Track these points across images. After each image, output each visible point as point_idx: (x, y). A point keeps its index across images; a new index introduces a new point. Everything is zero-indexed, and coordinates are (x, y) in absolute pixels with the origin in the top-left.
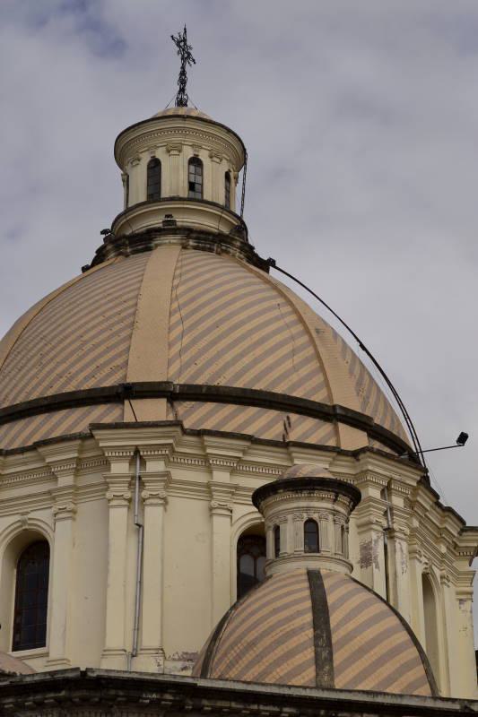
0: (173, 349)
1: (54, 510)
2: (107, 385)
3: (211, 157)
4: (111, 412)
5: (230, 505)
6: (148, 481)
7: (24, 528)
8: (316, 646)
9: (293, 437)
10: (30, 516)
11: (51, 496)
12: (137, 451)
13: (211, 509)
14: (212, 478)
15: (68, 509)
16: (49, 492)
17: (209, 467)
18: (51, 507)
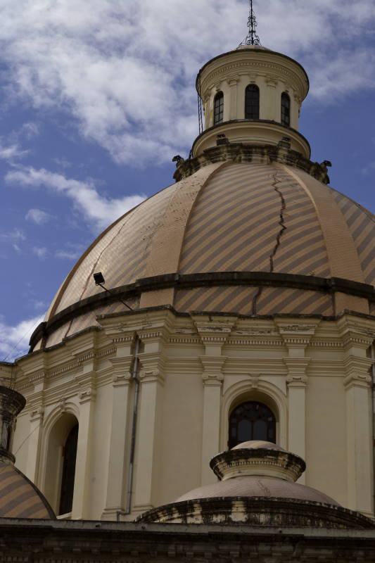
2: (190, 273)
3: (267, 82)
4: (201, 295)
7: (253, 387)
9: (249, 291)
12: (137, 337)
13: (287, 383)
15: (154, 374)
17: (285, 345)
18: (286, 375)
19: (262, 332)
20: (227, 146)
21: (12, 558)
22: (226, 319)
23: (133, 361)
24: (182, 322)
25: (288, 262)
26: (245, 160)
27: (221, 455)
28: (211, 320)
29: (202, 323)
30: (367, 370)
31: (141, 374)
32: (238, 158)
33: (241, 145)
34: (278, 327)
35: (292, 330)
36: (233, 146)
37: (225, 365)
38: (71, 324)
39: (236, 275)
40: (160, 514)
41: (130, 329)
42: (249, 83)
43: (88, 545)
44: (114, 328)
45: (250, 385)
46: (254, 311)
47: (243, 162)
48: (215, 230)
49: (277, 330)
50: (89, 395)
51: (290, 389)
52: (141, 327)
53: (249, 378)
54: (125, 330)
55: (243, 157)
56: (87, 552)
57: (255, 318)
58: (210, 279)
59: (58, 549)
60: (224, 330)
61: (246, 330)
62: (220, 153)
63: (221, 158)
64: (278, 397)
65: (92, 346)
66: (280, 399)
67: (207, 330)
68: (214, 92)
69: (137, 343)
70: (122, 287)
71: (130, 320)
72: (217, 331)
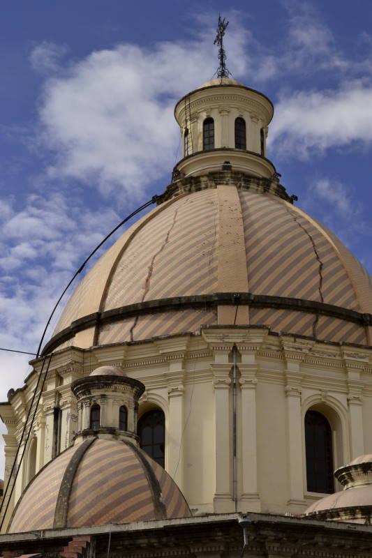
0: (251, 266)
5: (300, 389)
6: (244, 371)
8: (55, 515)
9: (309, 317)
10: (329, 394)
11: (167, 378)
12: (235, 348)
13: (348, 400)
14: (286, 368)
15: (253, 382)
16: (165, 375)
19: (330, 356)
20: (232, 173)
21: (203, 549)
22: (307, 341)
23: (233, 368)
24: (272, 339)
26: (244, 187)
28: (295, 341)
29: (288, 343)
31: (241, 381)
32: (239, 185)
33: (243, 174)
35: (353, 357)
36: (237, 173)
37: (304, 380)
38: (137, 320)
39: (299, 302)
40: (342, 513)
41: (230, 341)
42: (238, 116)
43: (343, 542)
44: (216, 338)
45: (321, 399)
46: (314, 334)
47: (242, 188)
49: (341, 355)
50: (180, 391)
51: (351, 406)
52: (241, 340)
53: (320, 393)
54: (226, 340)
55: (243, 185)
56: (341, 547)
57: (326, 344)
60: (304, 351)
62: (225, 177)
63: (225, 182)
64: (341, 410)
65: (184, 348)
67: (291, 349)
68: (204, 116)
69: (235, 352)
70: (192, 297)
72: (299, 351)
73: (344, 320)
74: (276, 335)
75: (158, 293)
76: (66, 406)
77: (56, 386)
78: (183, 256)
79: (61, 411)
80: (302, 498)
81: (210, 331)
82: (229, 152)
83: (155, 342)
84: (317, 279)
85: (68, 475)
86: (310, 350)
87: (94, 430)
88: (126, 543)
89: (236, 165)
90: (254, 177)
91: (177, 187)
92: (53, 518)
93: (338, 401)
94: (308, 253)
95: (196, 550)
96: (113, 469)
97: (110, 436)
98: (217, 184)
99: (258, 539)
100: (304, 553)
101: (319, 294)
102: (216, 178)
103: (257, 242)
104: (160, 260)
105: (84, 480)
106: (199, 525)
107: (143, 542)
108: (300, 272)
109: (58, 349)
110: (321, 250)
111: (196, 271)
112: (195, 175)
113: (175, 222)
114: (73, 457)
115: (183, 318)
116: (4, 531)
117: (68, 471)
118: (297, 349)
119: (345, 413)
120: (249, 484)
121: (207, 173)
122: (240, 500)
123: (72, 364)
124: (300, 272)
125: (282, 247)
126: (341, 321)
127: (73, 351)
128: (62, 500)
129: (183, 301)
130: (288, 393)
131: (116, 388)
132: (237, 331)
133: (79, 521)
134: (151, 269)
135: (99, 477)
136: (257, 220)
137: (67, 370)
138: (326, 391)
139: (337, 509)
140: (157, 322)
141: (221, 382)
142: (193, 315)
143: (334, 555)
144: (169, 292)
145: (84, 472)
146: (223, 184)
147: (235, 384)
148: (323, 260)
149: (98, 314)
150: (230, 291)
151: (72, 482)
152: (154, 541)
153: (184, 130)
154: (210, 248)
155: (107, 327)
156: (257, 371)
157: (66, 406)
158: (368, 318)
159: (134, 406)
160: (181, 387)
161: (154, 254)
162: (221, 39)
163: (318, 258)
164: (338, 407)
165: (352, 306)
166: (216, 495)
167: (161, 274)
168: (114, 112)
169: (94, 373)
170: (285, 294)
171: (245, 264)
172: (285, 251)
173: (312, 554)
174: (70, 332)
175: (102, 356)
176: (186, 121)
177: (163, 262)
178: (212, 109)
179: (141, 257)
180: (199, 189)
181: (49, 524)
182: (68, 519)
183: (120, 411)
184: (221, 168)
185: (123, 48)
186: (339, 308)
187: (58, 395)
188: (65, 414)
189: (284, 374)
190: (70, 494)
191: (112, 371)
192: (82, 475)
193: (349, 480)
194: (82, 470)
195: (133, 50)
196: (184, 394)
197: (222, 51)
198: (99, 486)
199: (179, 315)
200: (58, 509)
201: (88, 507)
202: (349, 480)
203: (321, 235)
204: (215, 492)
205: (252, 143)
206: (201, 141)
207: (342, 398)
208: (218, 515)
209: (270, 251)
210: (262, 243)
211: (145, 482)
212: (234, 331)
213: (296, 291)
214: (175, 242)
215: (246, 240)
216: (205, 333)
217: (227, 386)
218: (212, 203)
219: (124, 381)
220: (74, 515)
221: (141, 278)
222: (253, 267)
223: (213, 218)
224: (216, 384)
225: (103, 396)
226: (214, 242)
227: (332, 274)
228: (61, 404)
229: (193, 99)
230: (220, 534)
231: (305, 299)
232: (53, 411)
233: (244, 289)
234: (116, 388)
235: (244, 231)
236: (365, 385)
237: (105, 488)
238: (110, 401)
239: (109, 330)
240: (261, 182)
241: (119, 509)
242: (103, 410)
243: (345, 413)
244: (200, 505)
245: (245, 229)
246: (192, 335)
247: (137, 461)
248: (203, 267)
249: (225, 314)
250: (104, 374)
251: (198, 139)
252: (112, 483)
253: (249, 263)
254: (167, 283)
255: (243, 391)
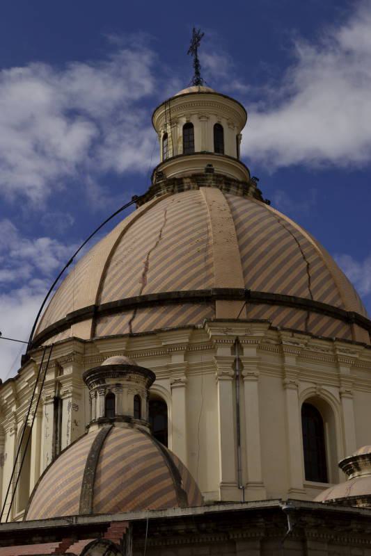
1: (172, 379)
5: (297, 381)
8: (81, 502)
9: (300, 314)
10: (323, 387)
11: (169, 370)
12: (237, 340)
13: (340, 393)
15: (230, 374)
16: (167, 367)
19: (323, 351)
20: (214, 175)
23: (235, 361)
24: (272, 334)
25: (260, 279)
26: (225, 189)
27: (367, 455)
28: (293, 336)
29: (286, 337)
30: (231, 365)
31: (244, 373)
33: (225, 177)
34: (336, 348)
36: (219, 176)
38: (135, 313)
40: (359, 501)
41: (234, 334)
44: (220, 331)
45: (315, 392)
48: (277, 255)
49: (334, 350)
51: (343, 399)
53: (314, 386)
54: (229, 334)
55: (224, 187)
57: (321, 339)
58: (274, 299)
59: (356, 530)
61: (313, 347)
62: (207, 180)
63: (207, 184)
65: (187, 340)
66: (336, 407)
68: (184, 121)
69: (237, 345)
71: (235, 327)
72: (296, 345)
73: (333, 317)
74: (274, 329)
75: (155, 286)
76: (68, 395)
77: (56, 376)
78: (179, 252)
79: (62, 400)
80: (301, 487)
81: (214, 324)
82: (209, 156)
83: (158, 335)
84: (305, 278)
85: (91, 461)
86: (306, 345)
87: (110, 417)
88: (164, 529)
89: (218, 169)
90: (234, 181)
91: (160, 188)
92: (78, 504)
93: (331, 394)
94: (295, 253)
95: (236, 537)
96: (134, 456)
97: (126, 424)
98: (199, 186)
99: (297, 525)
100: (338, 539)
101: (309, 292)
102: (199, 180)
103: (249, 241)
104: (156, 255)
105: (107, 467)
106: (240, 511)
107: (181, 528)
108: (289, 272)
109: (49, 342)
110: (306, 250)
111: (192, 267)
112: (177, 177)
113: (166, 220)
114: (94, 444)
115: (182, 312)
116: (3, 520)
117: (89, 458)
118: (294, 343)
119: (338, 405)
120: (254, 473)
121: (191, 175)
122: (246, 488)
123: (74, 354)
124: (289, 272)
125: (272, 246)
126: (330, 318)
127: (75, 342)
128: (86, 486)
129: (182, 296)
130: (287, 386)
131: (130, 377)
132: (240, 324)
133: (105, 507)
134: (147, 264)
135: (122, 465)
136: (246, 220)
137: (67, 360)
138: (320, 385)
139: (354, 497)
140: (156, 316)
141: (224, 374)
142: (192, 309)
143: (365, 540)
144: (166, 287)
145: (107, 460)
146: (205, 186)
147: (237, 376)
148: (310, 260)
149: (96, 307)
150: (227, 287)
151: (96, 469)
152: (193, 527)
153: (162, 134)
154: (204, 246)
155: (105, 319)
156: (258, 364)
157: (68, 395)
158: (354, 316)
159: (146, 396)
160: (184, 378)
161: (148, 250)
162: (196, 50)
163: (304, 258)
164: (332, 400)
165: (337, 304)
166: (222, 483)
167: (158, 268)
168: (24, 126)
169: (106, 363)
170: (278, 291)
171: (240, 261)
172: (274, 251)
173: (346, 540)
174: (65, 324)
175: (103, 348)
176: (166, 125)
177: (159, 257)
178: (191, 115)
179: (135, 252)
180: (181, 190)
181: (74, 510)
182: (94, 505)
183: (135, 400)
184: (204, 171)
185: (34, 66)
186: (328, 305)
187: (58, 384)
188: (66, 403)
189: (283, 368)
190: (94, 481)
191: (125, 361)
192: (104, 463)
193: (355, 469)
194: (104, 458)
195: (43, 69)
196: (187, 385)
197: (196, 61)
198: (123, 473)
199: (178, 309)
200: (83, 496)
201: (114, 494)
202: (355, 469)
203: (303, 237)
204: (221, 480)
205: (229, 149)
206: (181, 145)
207: (334, 391)
208: (247, 502)
209: (262, 249)
210: (253, 242)
211: (165, 470)
212: (237, 324)
213: (289, 288)
214: (168, 239)
215: (239, 238)
216: (209, 326)
217: (63, 397)
218: (200, 203)
219: (139, 371)
220: (100, 502)
221: (136, 273)
222: (247, 264)
223: (204, 217)
224: (220, 376)
225: (118, 385)
226: (208, 240)
227: (318, 273)
228: (61, 393)
229: (173, 105)
230: (262, 520)
231: (297, 296)
232: (53, 400)
233: (239, 285)
234: (130, 377)
235: (236, 230)
236: (355, 379)
237: (129, 475)
238: (125, 390)
239: (106, 322)
240: (240, 186)
241: (144, 496)
242: (118, 399)
243: (338, 405)
244: (206, 492)
245: (237, 228)
246: (194, 328)
247: (155, 449)
248: (199, 263)
249: (224, 309)
250: (117, 363)
251: (178, 142)
252: (135, 470)
253: (243, 260)
254: (163, 279)
255: (245, 383)
